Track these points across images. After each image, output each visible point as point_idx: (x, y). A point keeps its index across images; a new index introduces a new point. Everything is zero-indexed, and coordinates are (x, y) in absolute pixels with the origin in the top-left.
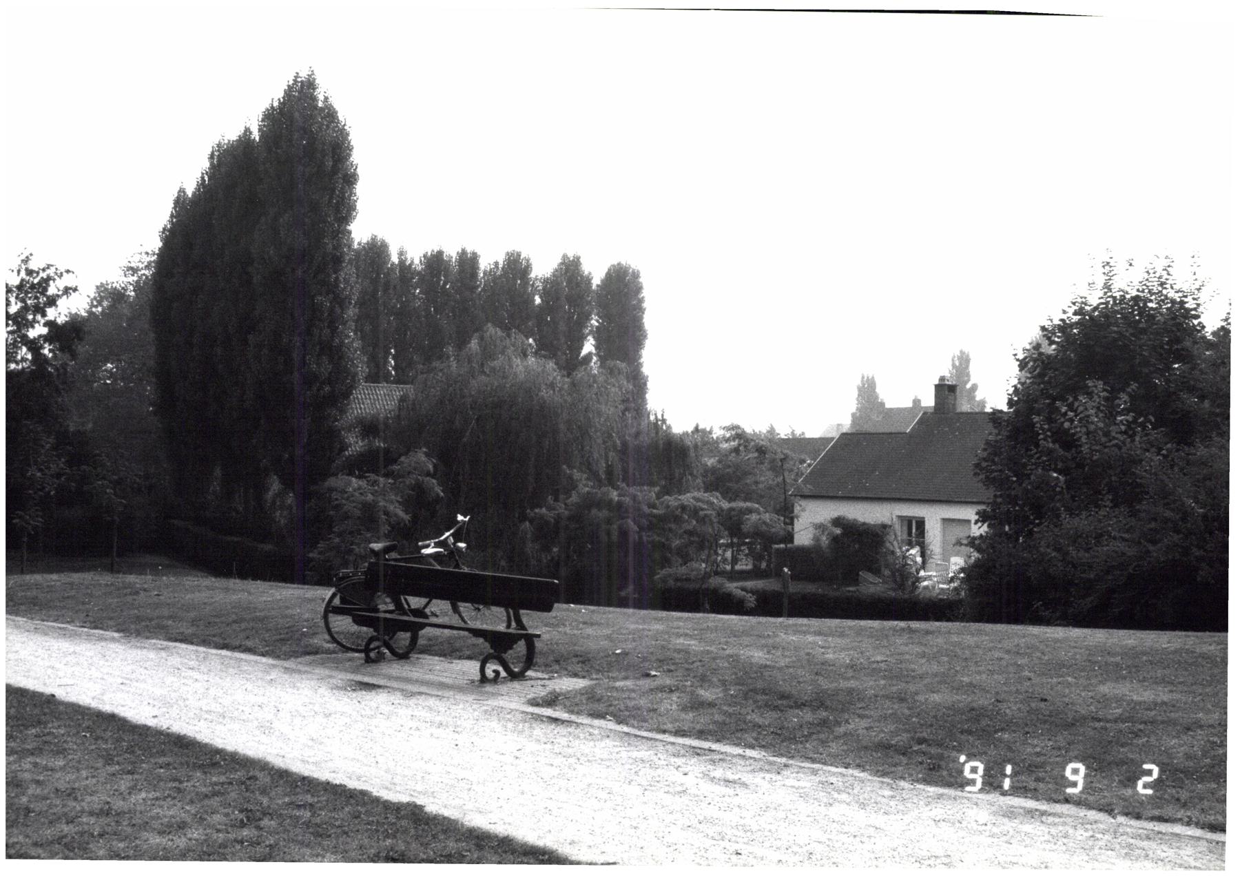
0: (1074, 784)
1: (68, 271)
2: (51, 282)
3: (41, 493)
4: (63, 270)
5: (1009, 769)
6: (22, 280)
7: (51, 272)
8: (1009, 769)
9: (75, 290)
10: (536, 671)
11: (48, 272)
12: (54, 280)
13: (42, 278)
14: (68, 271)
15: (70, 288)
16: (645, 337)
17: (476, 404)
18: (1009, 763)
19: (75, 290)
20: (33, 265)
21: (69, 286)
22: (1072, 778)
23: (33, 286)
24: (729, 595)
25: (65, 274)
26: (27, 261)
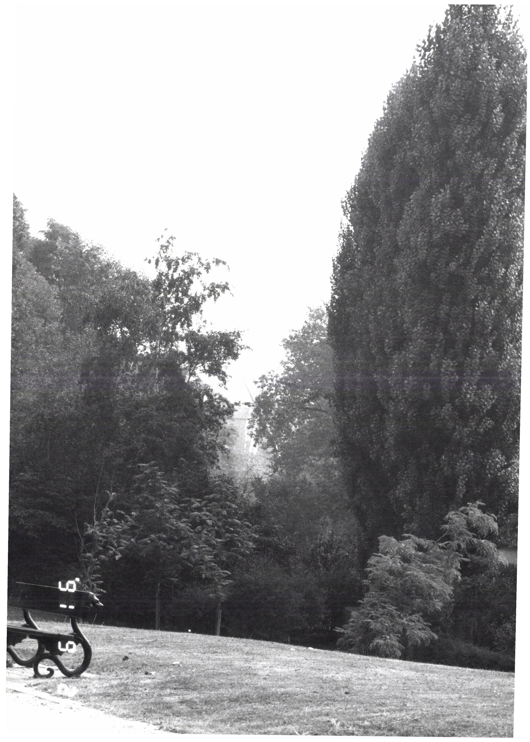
0: (64, 586)
1: (218, 262)
2: (194, 278)
3: (103, 557)
4: (210, 261)
5: (72, 607)
6: (161, 274)
7: (193, 263)
8: (72, 607)
9: (225, 288)
10: (89, 672)
11: (190, 263)
12: (199, 274)
13: (183, 271)
14: (218, 262)
15: (218, 286)
16: (391, 97)
17: (21, 230)
18: (75, 608)
19: (225, 288)
20: (174, 253)
21: (217, 282)
22: (67, 585)
23: (173, 283)
24: (229, 579)
25: (213, 265)
26: (167, 247)
